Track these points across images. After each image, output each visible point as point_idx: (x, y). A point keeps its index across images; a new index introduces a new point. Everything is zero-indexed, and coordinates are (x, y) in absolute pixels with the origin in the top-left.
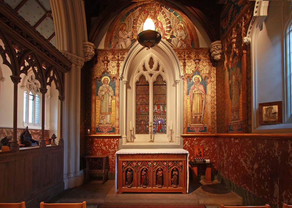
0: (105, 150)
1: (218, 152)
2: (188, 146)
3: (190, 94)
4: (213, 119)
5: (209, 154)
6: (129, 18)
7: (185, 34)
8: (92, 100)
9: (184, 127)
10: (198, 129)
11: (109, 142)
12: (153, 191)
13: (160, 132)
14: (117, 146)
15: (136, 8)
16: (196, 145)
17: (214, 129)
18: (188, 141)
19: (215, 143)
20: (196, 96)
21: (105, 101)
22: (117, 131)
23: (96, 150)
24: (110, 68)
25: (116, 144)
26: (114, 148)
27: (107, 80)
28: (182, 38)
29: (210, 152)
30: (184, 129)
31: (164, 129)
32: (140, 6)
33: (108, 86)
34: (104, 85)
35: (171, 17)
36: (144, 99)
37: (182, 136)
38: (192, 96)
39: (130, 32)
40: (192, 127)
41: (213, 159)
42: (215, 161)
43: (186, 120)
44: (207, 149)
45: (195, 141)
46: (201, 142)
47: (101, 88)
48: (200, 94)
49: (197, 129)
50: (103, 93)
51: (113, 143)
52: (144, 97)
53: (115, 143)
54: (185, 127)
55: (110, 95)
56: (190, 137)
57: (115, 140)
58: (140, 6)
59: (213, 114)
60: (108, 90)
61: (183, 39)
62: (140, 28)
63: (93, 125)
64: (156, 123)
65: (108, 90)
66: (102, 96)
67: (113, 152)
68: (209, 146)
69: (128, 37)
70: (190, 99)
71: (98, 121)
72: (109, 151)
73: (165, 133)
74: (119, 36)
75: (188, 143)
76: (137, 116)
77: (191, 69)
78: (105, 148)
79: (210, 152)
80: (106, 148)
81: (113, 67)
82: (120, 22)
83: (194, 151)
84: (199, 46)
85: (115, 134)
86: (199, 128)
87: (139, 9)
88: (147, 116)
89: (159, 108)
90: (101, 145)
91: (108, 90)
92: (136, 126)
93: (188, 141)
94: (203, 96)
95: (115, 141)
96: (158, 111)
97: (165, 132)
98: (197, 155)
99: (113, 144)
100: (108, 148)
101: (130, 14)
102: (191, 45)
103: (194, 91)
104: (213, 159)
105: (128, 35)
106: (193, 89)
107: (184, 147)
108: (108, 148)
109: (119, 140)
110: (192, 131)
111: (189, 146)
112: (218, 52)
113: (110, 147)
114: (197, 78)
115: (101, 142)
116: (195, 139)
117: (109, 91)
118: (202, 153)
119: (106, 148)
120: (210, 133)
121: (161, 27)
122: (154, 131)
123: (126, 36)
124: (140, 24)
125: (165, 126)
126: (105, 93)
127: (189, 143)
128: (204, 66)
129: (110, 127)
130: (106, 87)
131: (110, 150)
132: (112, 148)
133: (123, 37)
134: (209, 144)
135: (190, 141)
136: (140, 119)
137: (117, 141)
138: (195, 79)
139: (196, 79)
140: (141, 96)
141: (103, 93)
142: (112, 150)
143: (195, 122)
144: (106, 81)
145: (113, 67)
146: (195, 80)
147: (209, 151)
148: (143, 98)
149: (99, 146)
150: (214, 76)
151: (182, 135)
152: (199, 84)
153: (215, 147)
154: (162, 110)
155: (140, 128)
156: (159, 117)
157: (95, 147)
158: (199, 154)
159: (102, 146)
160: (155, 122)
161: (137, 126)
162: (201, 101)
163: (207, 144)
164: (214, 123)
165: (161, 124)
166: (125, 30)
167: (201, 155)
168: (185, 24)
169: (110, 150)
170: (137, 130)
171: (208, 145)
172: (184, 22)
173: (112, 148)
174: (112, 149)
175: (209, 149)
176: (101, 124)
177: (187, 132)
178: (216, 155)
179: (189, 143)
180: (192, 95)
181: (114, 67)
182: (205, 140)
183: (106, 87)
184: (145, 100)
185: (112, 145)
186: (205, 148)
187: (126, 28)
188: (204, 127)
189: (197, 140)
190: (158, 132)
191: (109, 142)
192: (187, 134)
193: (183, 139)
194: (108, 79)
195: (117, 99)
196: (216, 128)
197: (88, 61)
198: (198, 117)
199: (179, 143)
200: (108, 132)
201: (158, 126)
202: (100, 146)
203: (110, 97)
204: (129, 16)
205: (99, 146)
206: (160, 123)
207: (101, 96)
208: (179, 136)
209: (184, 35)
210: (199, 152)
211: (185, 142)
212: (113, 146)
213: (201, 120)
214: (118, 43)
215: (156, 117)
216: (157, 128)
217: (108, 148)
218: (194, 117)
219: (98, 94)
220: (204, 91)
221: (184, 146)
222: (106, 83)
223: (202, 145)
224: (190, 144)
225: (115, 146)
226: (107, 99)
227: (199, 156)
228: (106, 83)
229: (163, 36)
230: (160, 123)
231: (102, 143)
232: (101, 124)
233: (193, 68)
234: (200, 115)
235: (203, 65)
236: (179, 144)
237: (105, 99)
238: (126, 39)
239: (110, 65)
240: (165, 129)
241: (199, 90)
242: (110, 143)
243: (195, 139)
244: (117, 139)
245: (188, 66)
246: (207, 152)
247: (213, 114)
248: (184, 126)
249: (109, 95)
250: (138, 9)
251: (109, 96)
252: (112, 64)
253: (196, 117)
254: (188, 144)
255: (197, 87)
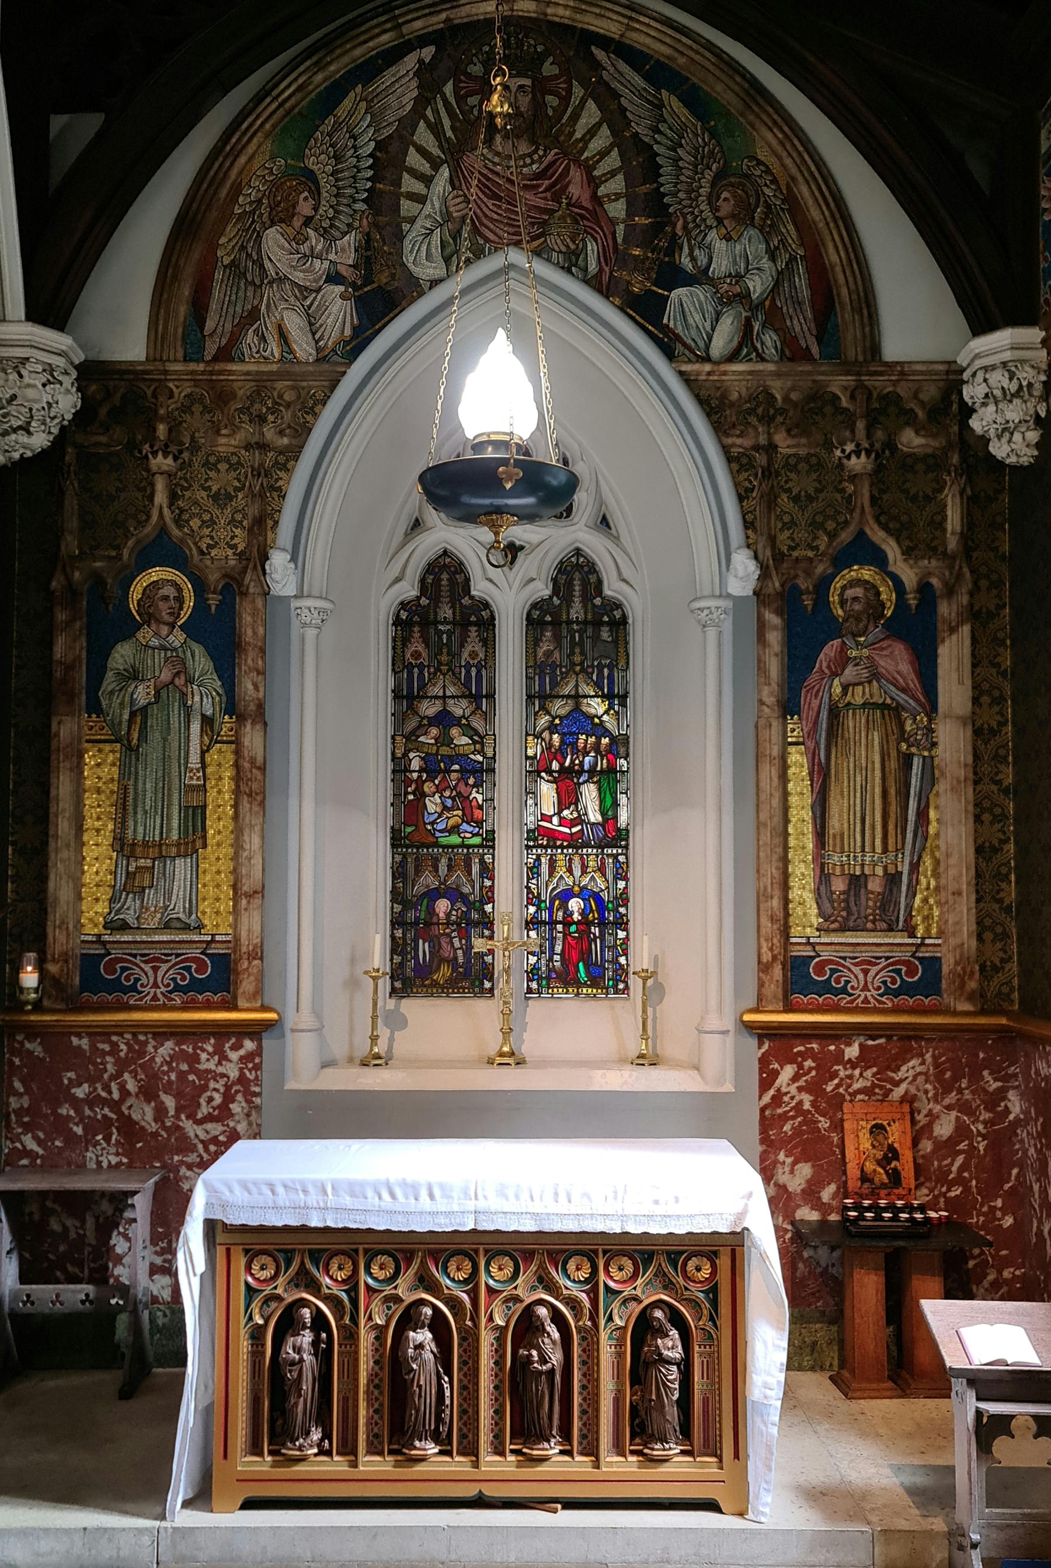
0: (153, 1127)
1: (1032, 1151)
2: (801, 1103)
3: (810, 703)
4: (988, 898)
5: (962, 1169)
6: (337, 127)
7: (773, 258)
8: (54, 744)
9: (767, 957)
10: (877, 975)
11: (184, 1067)
12: (491, 1491)
13: (578, 984)
14: (249, 1096)
15: (393, 56)
16: (859, 1091)
17: (1001, 977)
18: (800, 1067)
19: (1006, 1078)
20: (853, 723)
21: (152, 751)
22: (247, 985)
23: (79, 1130)
24: (196, 503)
25: (242, 1080)
26: (223, 1113)
27: (169, 591)
28: (751, 285)
29: (972, 1149)
30: (764, 968)
31: (608, 955)
32: (423, 41)
33: (177, 638)
34: (145, 635)
35: (662, 127)
36: (454, 731)
37: (763, 1033)
38: (824, 725)
39: (351, 239)
40: (825, 955)
41: (999, 1203)
42: (1008, 1221)
43: (776, 903)
44: (944, 1129)
45: (852, 1064)
46: (901, 1074)
47: (122, 655)
48: (883, 706)
49: (866, 972)
50: (142, 694)
51: (217, 1076)
52: (458, 712)
53: (234, 1074)
54: (774, 958)
55: (197, 706)
56: (816, 1037)
57: (232, 1048)
58: (423, 41)
59: (988, 860)
60: (178, 674)
61: (754, 297)
62: (428, 209)
63: (58, 940)
64: (545, 916)
65: (182, 669)
66: (133, 714)
67: (214, 1140)
68: (964, 1107)
69: (334, 278)
70: (811, 744)
71: (102, 907)
72: (185, 1137)
73: (596, 980)
74: (267, 264)
75: (795, 1079)
76: (398, 858)
77: (819, 518)
78: (149, 1110)
79: (972, 1148)
80: (160, 1113)
81: (216, 497)
82: (273, 158)
83: (842, 1140)
84: (874, 349)
85: (235, 1008)
86: (883, 963)
87: (421, 61)
88: (482, 862)
89: (568, 798)
90: (122, 1088)
91: (178, 674)
92: (393, 937)
93: (800, 1067)
94: (909, 726)
95: (234, 1056)
96: (563, 822)
97: (615, 986)
98: (865, 1178)
99: (212, 1084)
100: (179, 1109)
101: (347, 103)
102: (820, 341)
103: (837, 690)
104: (993, 1209)
105: (332, 257)
106: (835, 674)
107: (763, 1110)
108: (172, 1112)
109: (259, 1052)
110: (825, 988)
111: (807, 1099)
112: (1014, 412)
113: (188, 1106)
114: (858, 592)
115: (122, 1066)
116: (852, 1051)
117: (190, 681)
118: (907, 1155)
119: (160, 1113)
120: (965, 1006)
121: (586, 204)
122: (533, 973)
123: (320, 267)
124: (427, 181)
125: (621, 934)
126: (158, 693)
127: (801, 1083)
128: (914, 499)
129: (196, 952)
130: (166, 649)
131: (190, 1128)
132: (204, 1110)
133: (298, 277)
134: (960, 1091)
135: (809, 1063)
136: (428, 880)
137: (248, 1057)
138: (850, 593)
139: (855, 599)
140: (429, 708)
141: (142, 694)
142: (209, 1126)
143: (846, 919)
144: (162, 605)
145: (222, 498)
146: (843, 603)
147: (962, 1146)
148: (444, 719)
149: (104, 1094)
150: (994, 577)
151: (747, 1018)
152: (876, 632)
153: (1007, 1111)
154: (594, 816)
155: (424, 947)
156: (570, 870)
157: (75, 1103)
158: (879, 1163)
159: (125, 1093)
160: (539, 908)
161: (399, 933)
162: (893, 764)
163: (947, 1090)
164: (999, 930)
165: (585, 923)
166: (308, 221)
167: (895, 1178)
168: (774, 181)
169: (190, 1128)
170: (401, 965)
171: (951, 1098)
172: (759, 163)
173: (204, 1110)
174: (209, 1118)
175: (961, 1131)
176: (124, 927)
177: (786, 997)
178: (1015, 1171)
179: (801, 1083)
180: (824, 715)
181: (230, 498)
182: (928, 1057)
183: (166, 649)
184: (465, 740)
185: (204, 1088)
186: (932, 1117)
187: (316, 209)
188: (921, 960)
189: (865, 1059)
190: (567, 979)
191: (184, 1067)
192: (789, 1009)
193: (760, 1045)
194: (179, 590)
195: (246, 742)
196: (1014, 967)
197: (29, 454)
198: (875, 885)
199: (730, 1074)
200: (177, 988)
201: (566, 934)
202: (116, 1095)
203: (196, 727)
204: (342, 111)
205: (104, 1094)
206: (576, 917)
207: (126, 717)
208: (729, 1023)
209: (766, 263)
210: (880, 1155)
211: (776, 1074)
212: (211, 1099)
213: (897, 903)
214: (253, 316)
215: (545, 868)
216: (552, 952)
217: (172, 1112)
218: (839, 885)
219: (104, 703)
220: (914, 683)
221: (767, 1098)
222: (167, 618)
223: (908, 1099)
224: (814, 1088)
225: (228, 1098)
226: (174, 738)
227: (884, 1186)
228: (167, 618)
229: (601, 270)
230: (576, 917)
231: (126, 1076)
232: (124, 927)
233: (830, 512)
234: (891, 870)
235: (906, 492)
236: (729, 1087)
237: (155, 737)
238: (319, 290)
239: (196, 486)
240: (615, 961)
241: (875, 675)
242: (192, 1070)
243: (852, 1051)
244: (249, 1045)
245: (796, 499)
246: (947, 1147)
247: (988, 860)
248: (764, 949)
249: (188, 711)
250: (410, 61)
251: (188, 716)
252: (212, 474)
253: (857, 882)
254: (800, 1089)
255: (865, 652)
